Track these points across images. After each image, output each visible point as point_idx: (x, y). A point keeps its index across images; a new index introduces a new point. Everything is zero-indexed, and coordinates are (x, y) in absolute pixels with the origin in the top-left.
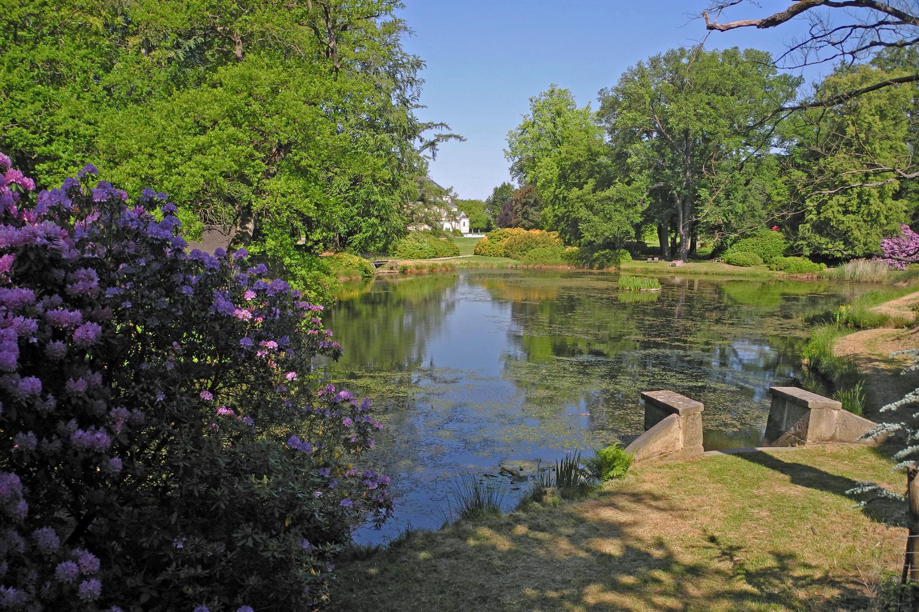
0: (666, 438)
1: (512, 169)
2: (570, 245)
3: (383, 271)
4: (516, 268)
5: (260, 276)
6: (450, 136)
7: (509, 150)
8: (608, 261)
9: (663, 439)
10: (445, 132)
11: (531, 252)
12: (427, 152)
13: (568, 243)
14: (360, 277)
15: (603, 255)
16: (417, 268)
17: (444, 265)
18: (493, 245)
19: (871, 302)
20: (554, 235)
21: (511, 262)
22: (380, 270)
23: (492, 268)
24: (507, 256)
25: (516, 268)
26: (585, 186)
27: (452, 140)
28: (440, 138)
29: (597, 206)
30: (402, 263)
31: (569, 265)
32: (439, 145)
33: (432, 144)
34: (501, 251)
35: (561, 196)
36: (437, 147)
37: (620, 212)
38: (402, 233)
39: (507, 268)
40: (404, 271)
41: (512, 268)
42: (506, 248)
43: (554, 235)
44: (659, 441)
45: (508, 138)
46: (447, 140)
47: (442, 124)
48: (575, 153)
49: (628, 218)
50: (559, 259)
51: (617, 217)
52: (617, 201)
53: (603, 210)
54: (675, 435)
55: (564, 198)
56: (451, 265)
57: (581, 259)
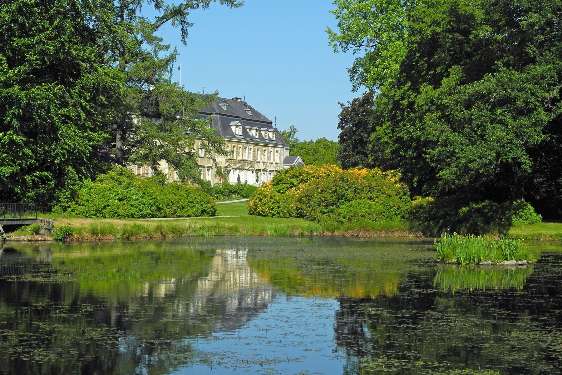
1: (354, 71)
2: (420, 194)
7: (337, 31)
8: (487, 221)
11: (344, 208)
12: (169, 32)
13: (415, 191)
15: (478, 211)
16: (94, 232)
17: (159, 229)
18: (278, 196)
19: (66, 260)
20: (393, 178)
21: (304, 223)
22: (13, 236)
23: (262, 235)
24: (301, 215)
26: (445, 80)
29: (459, 114)
30: (78, 223)
31: (411, 230)
32: (192, 15)
34: (291, 207)
35: (405, 102)
36: (188, 19)
37: (503, 123)
38: (95, 163)
40: (66, 238)
42: (300, 201)
43: (393, 178)
45: (335, 8)
48: (427, 20)
49: (517, 135)
50: (397, 220)
51: (496, 132)
52: (501, 102)
53: (469, 121)
55: (411, 105)
56: (174, 230)
57: (434, 218)
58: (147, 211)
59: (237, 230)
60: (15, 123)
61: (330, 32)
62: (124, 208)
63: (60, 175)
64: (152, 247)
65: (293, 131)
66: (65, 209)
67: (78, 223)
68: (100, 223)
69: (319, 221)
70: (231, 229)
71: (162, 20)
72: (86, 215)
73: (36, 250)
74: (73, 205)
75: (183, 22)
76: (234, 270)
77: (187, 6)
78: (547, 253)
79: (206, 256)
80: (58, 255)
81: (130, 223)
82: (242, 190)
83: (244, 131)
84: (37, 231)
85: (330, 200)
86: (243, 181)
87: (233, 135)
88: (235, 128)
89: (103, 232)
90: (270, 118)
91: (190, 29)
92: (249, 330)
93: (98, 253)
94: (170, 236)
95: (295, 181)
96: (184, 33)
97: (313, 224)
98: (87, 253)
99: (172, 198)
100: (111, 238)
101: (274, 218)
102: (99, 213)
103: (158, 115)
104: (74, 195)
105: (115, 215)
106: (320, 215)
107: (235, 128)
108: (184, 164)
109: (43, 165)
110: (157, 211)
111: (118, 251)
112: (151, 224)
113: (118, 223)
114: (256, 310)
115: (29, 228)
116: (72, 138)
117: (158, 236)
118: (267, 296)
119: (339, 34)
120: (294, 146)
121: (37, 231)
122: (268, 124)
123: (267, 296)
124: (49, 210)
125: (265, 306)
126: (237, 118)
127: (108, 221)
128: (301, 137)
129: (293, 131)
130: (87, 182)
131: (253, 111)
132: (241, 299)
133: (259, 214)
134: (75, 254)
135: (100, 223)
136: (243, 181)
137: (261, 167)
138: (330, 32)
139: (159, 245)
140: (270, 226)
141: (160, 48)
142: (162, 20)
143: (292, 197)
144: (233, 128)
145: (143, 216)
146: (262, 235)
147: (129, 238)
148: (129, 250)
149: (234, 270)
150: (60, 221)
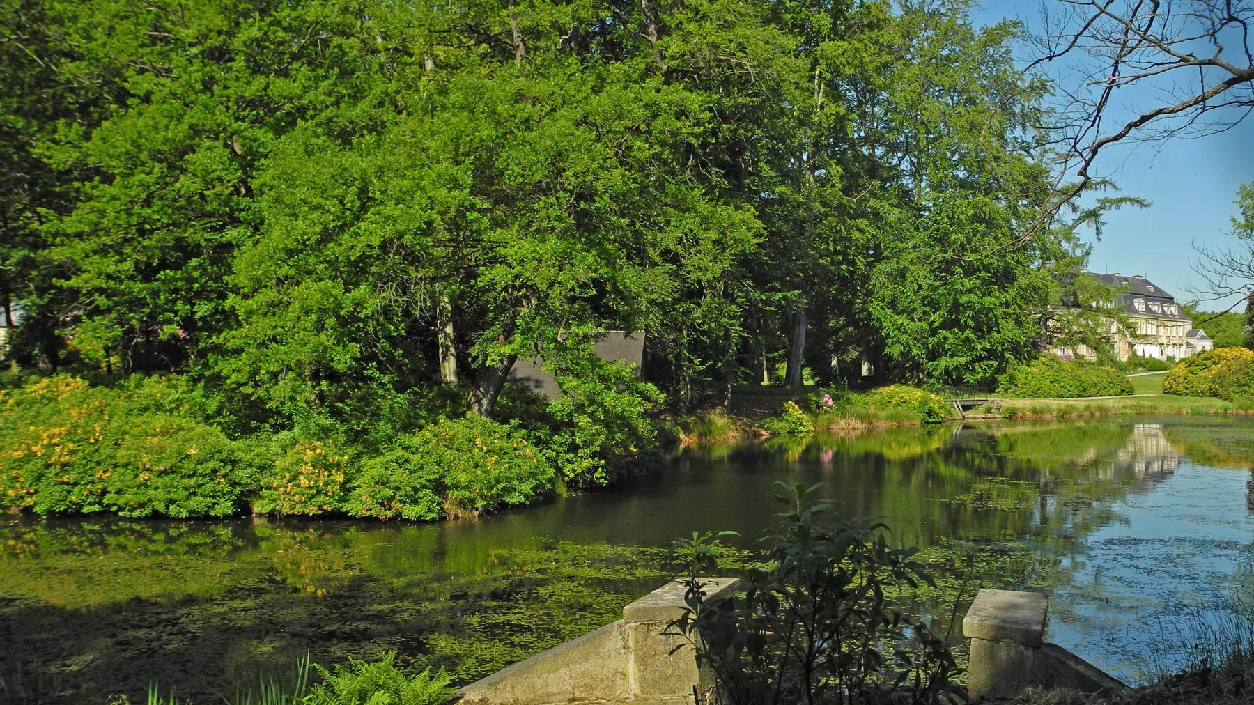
0: (585, 666)
3: (975, 416)
4: (1225, 415)
5: (239, 449)
6: (1122, 200)
7: (1242, 219)
9: (575, 669)
10: (1111, 194)
12: (1085, 232)
14: (918, 423)
16: (1034, 411)
17: (1087, 408)
18: (1191, 377)
21: (1218, 403)
22: (970, 414)
23: (1179, 413)
24: (1214, 395)
25: (1225, 415)
27: (1126, 206)
28: (1105, 204)
30: (1023, 404)
32: (1105, 216)
33: (1093, 214)
34: (1205, 386)
36: (1102, 219)
38: (1028, 351)
39: (1207, 414)
40: (1011, 416)
41: (1216, 414)
42: (1213, 381)
44: (563, 672)
45: (1239, 198)
46: (1118, 208)
47: (1104, 182)
54: (612, 664)
56: (1100, 409)
58: (1074, 392)
59: (1156, 408)
60: (970, 322)
61: (1234, 220)
62: (1056, 388)
63: (1002, 360)
64: (1082, 424)
65: (1195, 303)
66: (1006, 391)
67: (1023, 404)
68: (1040, 403)
69: (1232, 401)
70: (1150, 407)
71: (1080, 220)
72: (1024, 396)
73: (989, 426)
74: (1013, 388)
75: (1097, 222)
76: (1150, 442)
77: (1101, 208)
78: (1014, 623)
79: (1126, 430)
80: (1005, 430)
81: (1063, 403)
82: (1152, 365)
83: (1147, 306)
84: (989, 410)
85: (1243, 381)
86: (1147, 355)
87: (1136, 311)
88: (1139, 305)
89: (1042, 411)
90: (1173, 295)
91: (1103, 228)
92: (1157, 495)
93: (1038, 428)
94: (1097, 414)
95: (1206, 362)
96: (1098, 232)
97: (1227, 403)
98: (1028, 428)
99: (1096, 380)
100: (1049, 416)
101: (1189, 397)
102: (1035, 394)
103: (1077, 305)
104: (1012, 380)
105: (1049, 395)
106: (1233, 395)
107: (1139, 305)
108: (1101, 344)
109: (991, 354)
110: (1083, 392)
111: (1054, 427)
112: (1080, 403)
113: (1054, 403)
114: (1164, 475)
115: (981, 408)
116: (1009, 330)
117: (1087, 414)
118: (1173, 464)
119: (1243, 222)
120: (1195, 318)
121: (989, 410)
122: (1169, 300)
123: (1173, 464)
124: (992, 391)
125: (1171, 472)
126: (1140, 295)
127: (1044, 401)
128: (1205, 307)
129: (1195, 303)
130: (1024, 368)
131: (1155, 288)
132: (1148, 465)
133: (1174, 393)
134: (1019, 429)
135: (1040, 403)
136: (1147, 355)
137: (1165, 341)
138: (1234, 220)
139: (1087, 422)
140: (1188, 405)
141: (1076, 246)
142: (1080, 220)
143: (1205, 378)
144: (1136, 305)
145: (1071, 396)
146: (1179, 413)
147: (1063, 416)
148: (1063, 426)
149: (1150, 442)
150: (1003, 401)
